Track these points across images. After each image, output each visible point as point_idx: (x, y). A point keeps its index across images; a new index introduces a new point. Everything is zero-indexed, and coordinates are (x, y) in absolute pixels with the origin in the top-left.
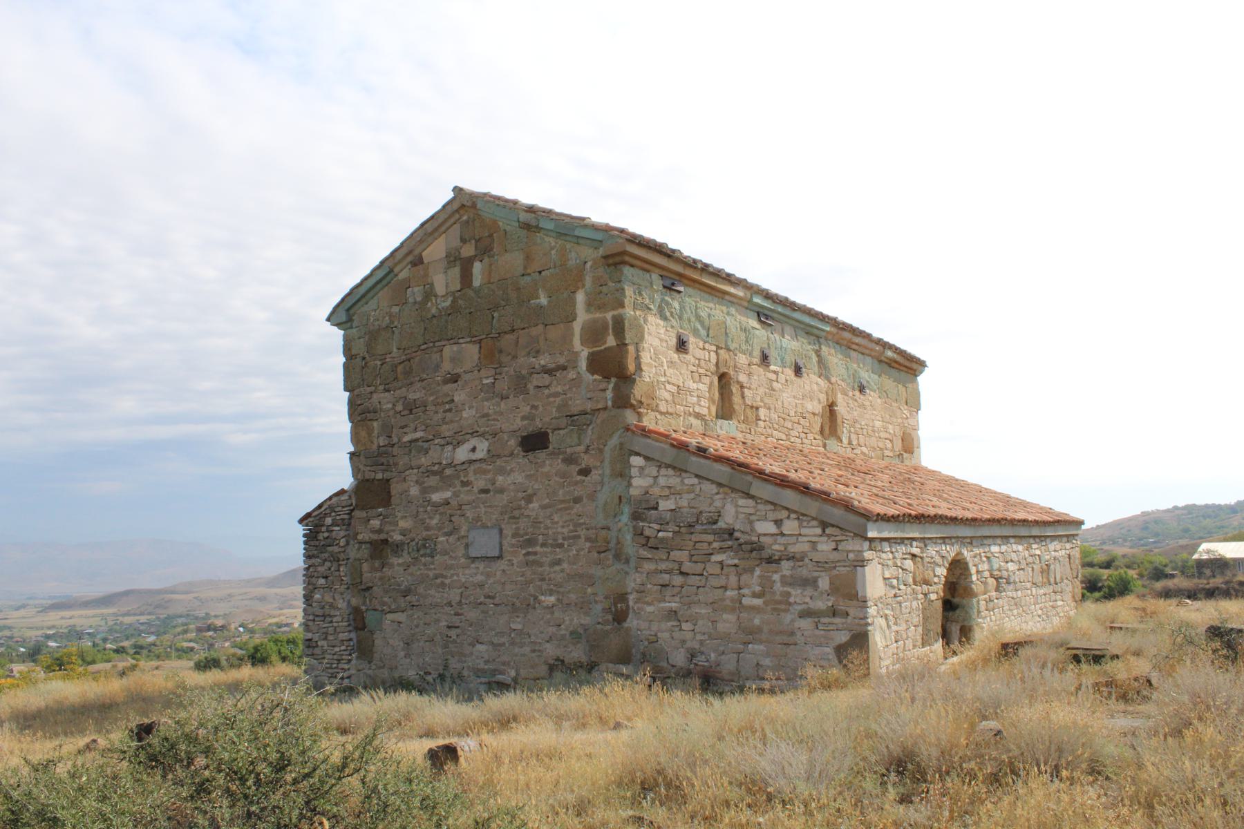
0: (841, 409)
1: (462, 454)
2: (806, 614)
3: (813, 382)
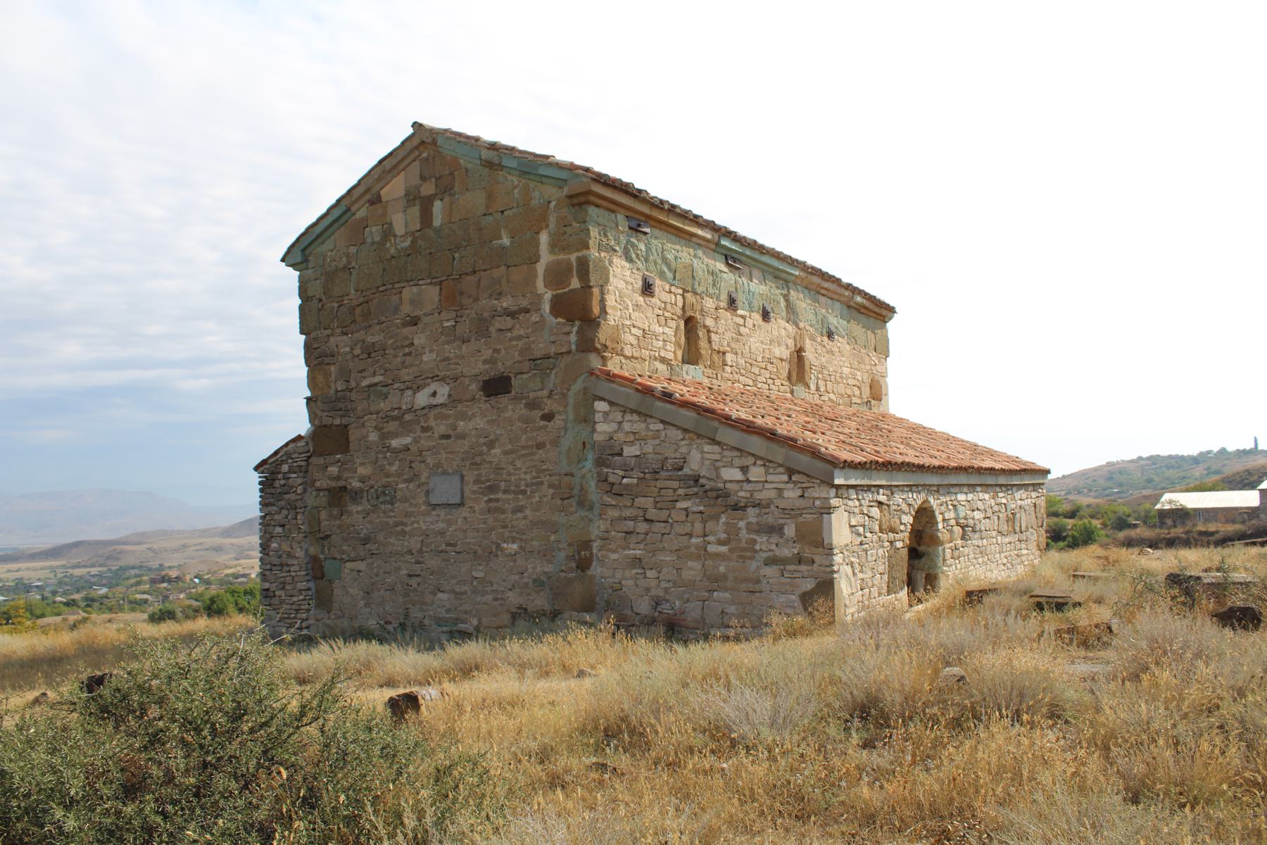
0: (809, 355)
1: (422, 398)
2: (772, 561)
3: (780, 327)
